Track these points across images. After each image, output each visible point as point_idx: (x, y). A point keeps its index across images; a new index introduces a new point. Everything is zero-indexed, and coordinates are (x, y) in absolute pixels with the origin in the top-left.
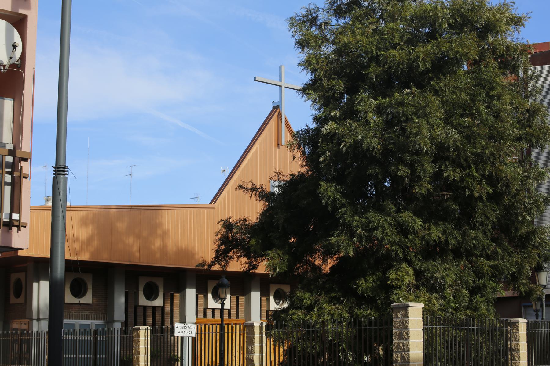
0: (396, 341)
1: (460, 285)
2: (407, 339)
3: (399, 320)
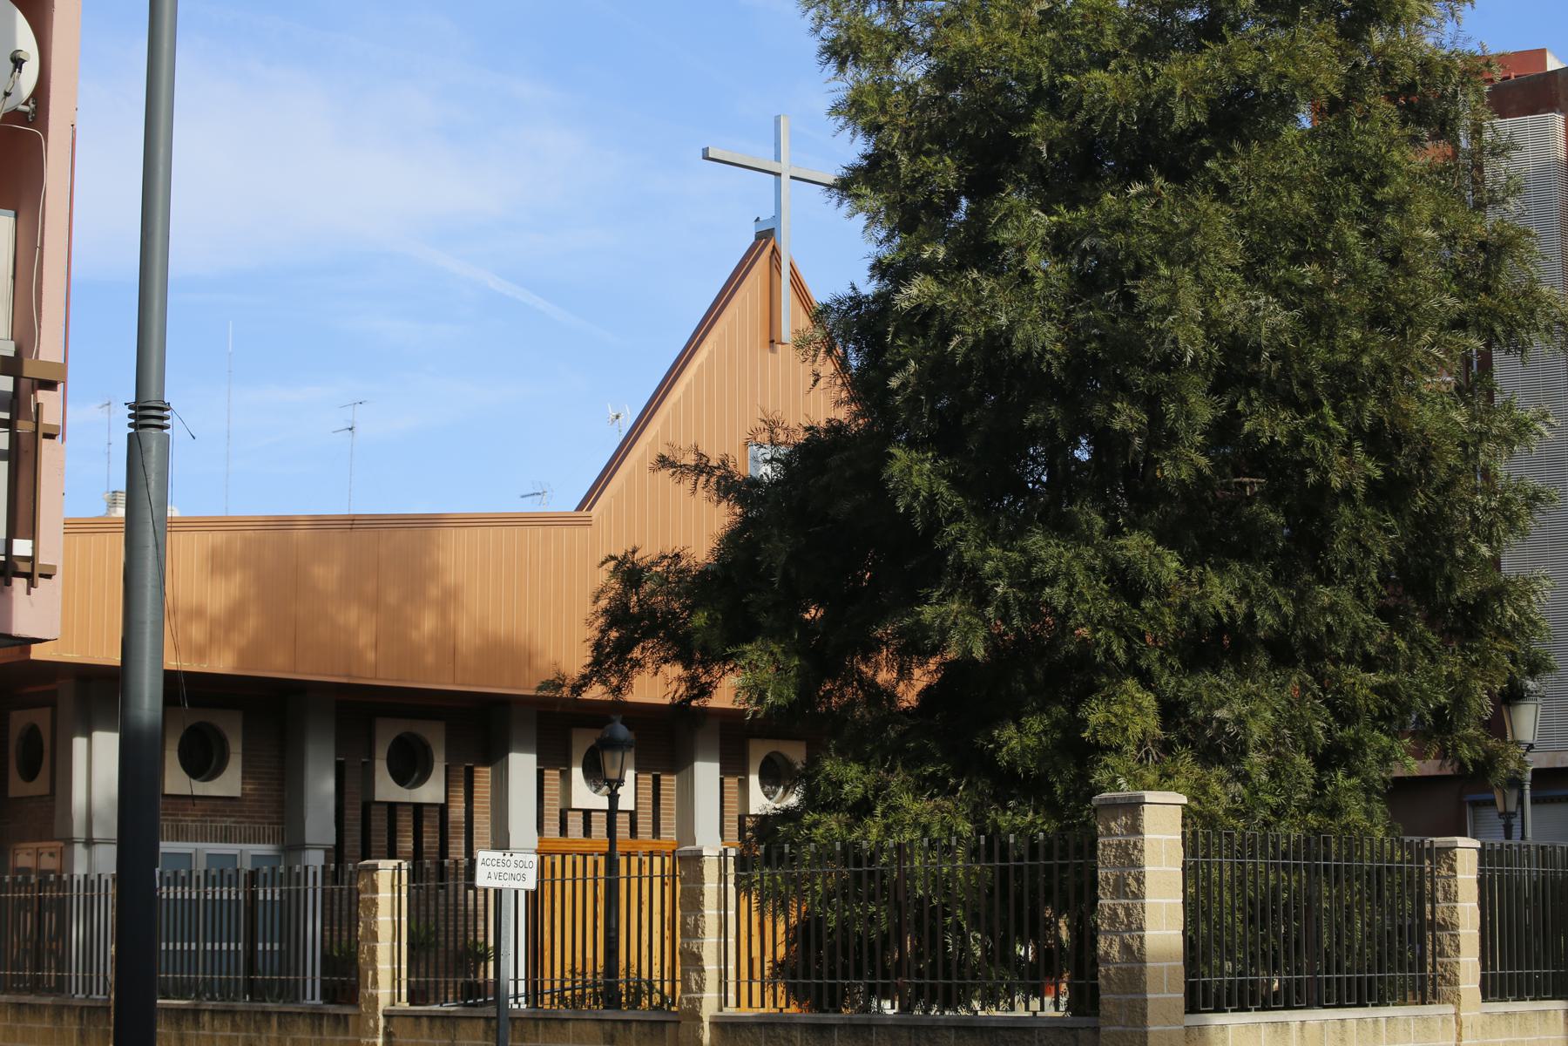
0: (1105, 901)
1: (1288, 741)
2: (1139, 896)
3: (1114, 840)
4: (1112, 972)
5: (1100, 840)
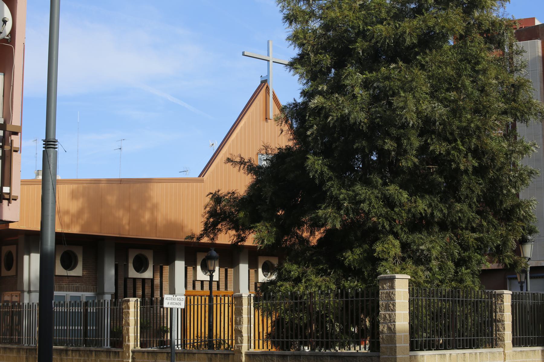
0: (382, 312)
1: (445, 257)
2: (394, 310)
3: (385, 291)
4: (384, 337)
5: (380, 291)
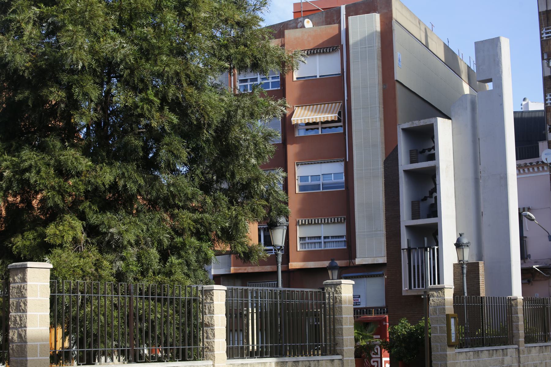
0: (12, 314)
1: (150, 243)
2: (25, 311)
3: (16, 285)
4: (14, 347)
5: (11, 285)
